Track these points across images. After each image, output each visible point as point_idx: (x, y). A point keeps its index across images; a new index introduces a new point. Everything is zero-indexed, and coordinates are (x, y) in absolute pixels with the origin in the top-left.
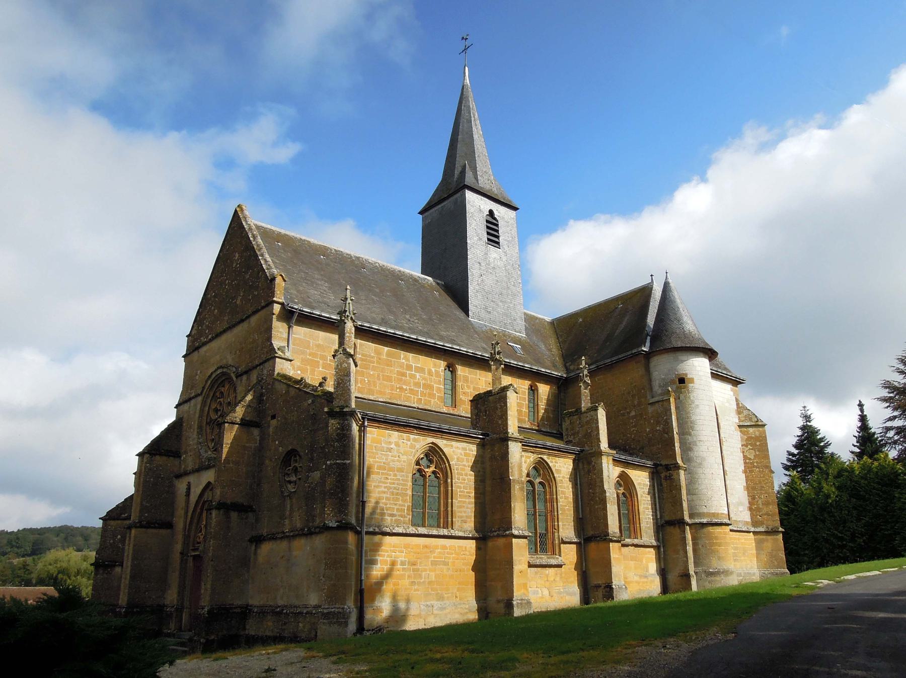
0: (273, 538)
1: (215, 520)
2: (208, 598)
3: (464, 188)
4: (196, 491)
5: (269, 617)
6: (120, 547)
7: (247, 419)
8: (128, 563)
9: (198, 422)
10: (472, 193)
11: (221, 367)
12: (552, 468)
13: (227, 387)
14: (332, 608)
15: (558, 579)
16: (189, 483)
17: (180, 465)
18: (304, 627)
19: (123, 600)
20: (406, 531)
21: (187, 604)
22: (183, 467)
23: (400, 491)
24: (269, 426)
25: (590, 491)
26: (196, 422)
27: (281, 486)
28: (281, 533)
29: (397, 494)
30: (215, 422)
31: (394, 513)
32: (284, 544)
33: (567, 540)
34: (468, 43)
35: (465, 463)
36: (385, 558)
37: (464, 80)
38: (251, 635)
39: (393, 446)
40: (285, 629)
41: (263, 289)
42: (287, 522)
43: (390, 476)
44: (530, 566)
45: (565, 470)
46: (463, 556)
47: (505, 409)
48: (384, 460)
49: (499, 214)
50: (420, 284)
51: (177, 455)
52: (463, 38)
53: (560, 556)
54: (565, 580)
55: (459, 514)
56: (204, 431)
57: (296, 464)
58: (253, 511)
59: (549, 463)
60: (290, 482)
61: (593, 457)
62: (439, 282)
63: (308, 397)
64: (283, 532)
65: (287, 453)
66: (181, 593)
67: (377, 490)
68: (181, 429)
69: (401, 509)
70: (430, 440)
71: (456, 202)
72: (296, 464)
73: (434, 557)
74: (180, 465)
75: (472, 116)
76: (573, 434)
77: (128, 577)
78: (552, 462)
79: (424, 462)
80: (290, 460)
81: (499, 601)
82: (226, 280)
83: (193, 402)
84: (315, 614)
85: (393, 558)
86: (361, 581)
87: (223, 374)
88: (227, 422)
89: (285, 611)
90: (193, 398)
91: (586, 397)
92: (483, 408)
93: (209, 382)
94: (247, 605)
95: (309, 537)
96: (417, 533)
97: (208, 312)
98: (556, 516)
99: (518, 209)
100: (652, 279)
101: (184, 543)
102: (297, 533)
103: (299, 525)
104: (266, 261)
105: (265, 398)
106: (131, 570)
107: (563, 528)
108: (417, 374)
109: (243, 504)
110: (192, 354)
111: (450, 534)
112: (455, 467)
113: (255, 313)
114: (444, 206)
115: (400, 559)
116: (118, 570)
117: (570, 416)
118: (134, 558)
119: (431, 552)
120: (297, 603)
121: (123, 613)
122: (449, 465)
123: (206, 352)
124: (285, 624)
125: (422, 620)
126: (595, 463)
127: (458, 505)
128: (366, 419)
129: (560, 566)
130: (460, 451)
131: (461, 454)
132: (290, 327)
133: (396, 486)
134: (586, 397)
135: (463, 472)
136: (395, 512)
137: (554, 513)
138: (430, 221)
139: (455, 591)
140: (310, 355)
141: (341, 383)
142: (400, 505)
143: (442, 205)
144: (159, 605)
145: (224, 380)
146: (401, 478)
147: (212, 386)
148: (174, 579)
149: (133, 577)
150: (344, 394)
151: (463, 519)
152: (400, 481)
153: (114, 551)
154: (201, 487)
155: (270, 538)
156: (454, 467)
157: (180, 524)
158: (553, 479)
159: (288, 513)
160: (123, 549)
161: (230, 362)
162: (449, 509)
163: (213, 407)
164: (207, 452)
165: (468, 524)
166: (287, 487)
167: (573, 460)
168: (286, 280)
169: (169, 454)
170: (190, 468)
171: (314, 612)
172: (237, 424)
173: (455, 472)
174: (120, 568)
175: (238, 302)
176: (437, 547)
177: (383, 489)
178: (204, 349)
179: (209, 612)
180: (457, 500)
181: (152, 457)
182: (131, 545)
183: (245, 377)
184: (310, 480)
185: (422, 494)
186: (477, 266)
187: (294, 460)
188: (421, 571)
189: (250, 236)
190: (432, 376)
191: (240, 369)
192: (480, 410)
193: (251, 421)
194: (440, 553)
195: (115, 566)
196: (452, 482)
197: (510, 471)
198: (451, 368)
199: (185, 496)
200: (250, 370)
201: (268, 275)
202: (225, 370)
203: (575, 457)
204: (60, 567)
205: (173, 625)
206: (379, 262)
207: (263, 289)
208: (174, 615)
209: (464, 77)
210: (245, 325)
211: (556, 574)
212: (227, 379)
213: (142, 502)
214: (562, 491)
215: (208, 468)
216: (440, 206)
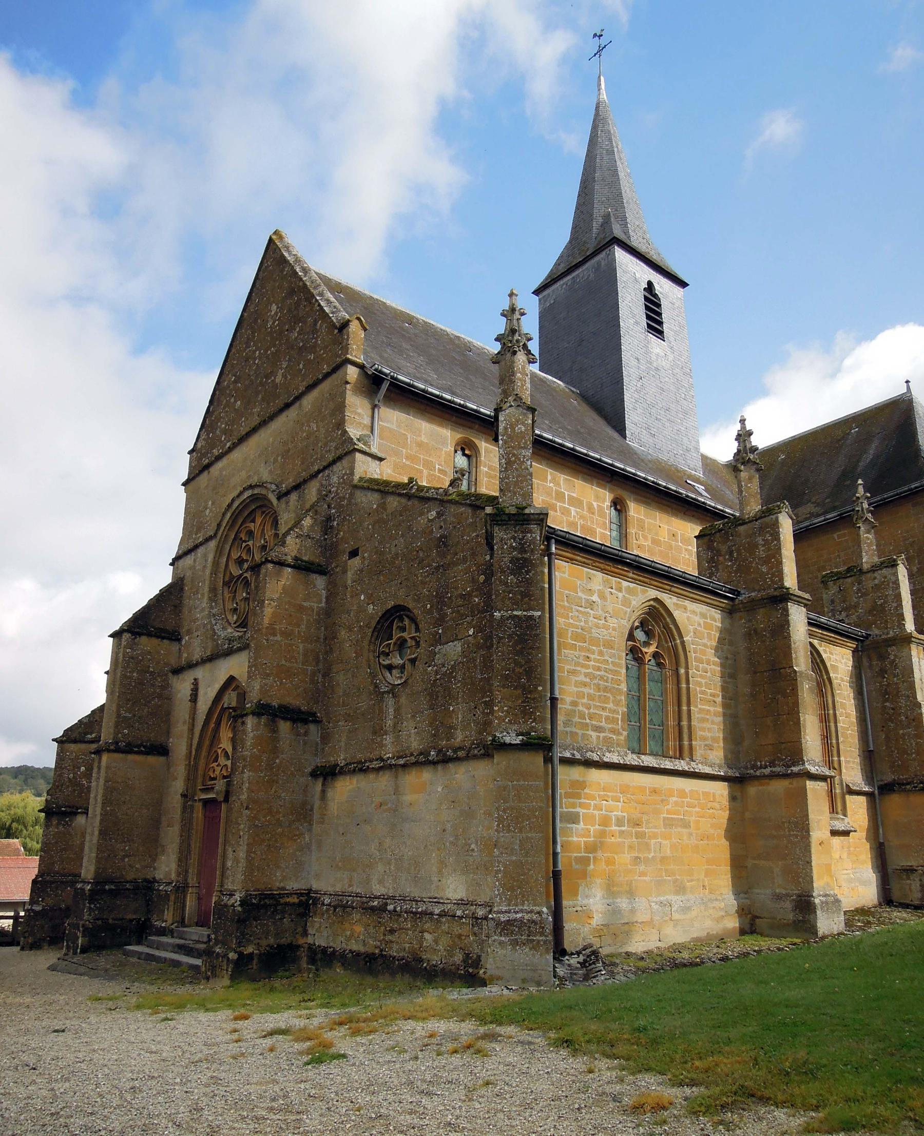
0: (361, 770)
1: (251, 735)
2: (240, 877)
3: (612, 244)
4: (207, 695)
5: (356, 916)
7: (305, 558)
8: (96, 808)
9: (211, 581)
10: (624, 253)
11: (251, 487)
12: (826, 661)
13: (259, 520)
14: (516, 913)
15: (845, 856)
16: (195, 679)
17: (180, 652)
18: (436, 941)
19: (88, 870)
20: (625, 760)
21: (192, 880)
22: (185, 655)
23: (609, 684)
24: (345, 572)
25: (887, 704)
26: (207, 583)
27: (373, 676)
28: (377, 760)
29: (606, 689)
30: (238, 579)
31: (602, 724)
32: (384, 781)
33: (855, 788)
34: (603, 41)
35: (705, 641)
36: (591, 811)
37: (599, 94)
38: (319, 946)
39: (595, 598)
40: (391, 942)
41: (326, 347)
42: (388, 740)
43: (593, 653)
44: (834, 833)
45: (843, 667)
46: (711, 811)
47: (775, 545)
48: (582, 624)
49: (660, 290)
50: (549, 386)
51: (174, 636)
53: (845, 815)
54: (855, 858)
55: (701, 733)
56: (220, 597)
57: (405, 635)
58: (317, 721)
59: (822, 653)
60: (390, 668)
61: (890, 646)
62: (572, 389)
63: (427, 508)
64: (382, 759)
65: (383, 615)
66: (183, 859)
67: (574, 678)
68: (181, 597)
69: (613, 717)
70: (653, 593)
71: (598, 268)
72: (405, 635)
73: (668, 812)
74: (180, 652)
75: (614, 145)
76: (846, 609)
77: (96, 833)
78: (825, 651)
79: (640, 635)
80: (390, 626)
81: (778, 897)
82: (255, 352)
83: (201, 551)
84: (461, 918)
85: (604, 812)
86: (555, 854)
87: (254, 498)
88: (272, 562)
89: (390, 907)
90: (201, 544)
91: (869, 545)
92: (724, 548)
93: (229, 515)
95: (440, 767)
96: (642, 764)
97: (224, 408)
98: (835, 745)
99: (688, 285)
100: (908, 388)
101: (188, 779)
102: (413, 759)
103: (415, 744)
104: (329, 302)
105: (335, 523)
106: (102, 820)
107: (846, 767)
108: (572, 509)
109: (300, 710)
110: (197, 479)
111: (692, 770)
112: (692, 646)
113: (311, 387)
114: (578, 275)
115: (615, 813)
116: (80, 820)
117: (838, 579)
119: (662, 801)
120: (416, 893)
121: (87, 892)
122: (683, 643)
123: (221, 470)
124: (392, 931)
125: (654, 931)
126: (895, 656)
127: (699, 716)
128: (553, 541)
129: (846, 833)
130: (697, 618)
131: (699, 625)
132: (374, 407)
133: (602, 673)
134: (869, 545)
135: (704, 657)
136: (603, 724)
137: (831, 739)
138: (552, 302)
139: (702, 876)
140: (407, 458)
141: (515, 462)
142: (611, 711)
143: (574, 274)
144: (146, 880)
145: (254, 510)
146: (610, 660)
148: (171, 836)
149: (103, 833)
150: (522, 482)
151: (707, 743)
152: (608, 665)
153: (74, 790)
154: (217, 686)
155: (354, 770)
156: (691, 647)
157: (180, 746)
158: (826, 681)
159: (389, 723)
160: (89, 788)
161: (266, 476)
162: (684, 723)
163: (235, 555)
164: (226, 630)
165: (714, 753)
166: (384, 678)
167: (853, 652)
168: (367, 327)
169: (163, 635)
170: (196, 657)
171: (459, 913)
172: (289, 566)
173: (692, 656)
174: (85, 816)
175: (279, 379)
176: (670, 793)
177: (582, 678)
178: (219, 465)
179: (243, 903)
180: (696, 707)
181: (136, 638)
182: (102, 781)
183: (294, 497)
184: (438, 659)
185: (638, 694)
186: (635, 363)
187: (398, 627)
188: (650, 838)
189: (298, 270)
190: (593, 513)
191: (284, 486)
192: (719, 551)
193: (311, 563)
194: (676, 803)
195: (76, 814)
196: (687, 674)
197: (794, 656)
198: (618, 505)
199: (190, 701)
200: (305, 481)
201: (335, 321)
202: (256, 491)
203: (857, 645)
204: (15, 814)
206: (487, 348)
207: (326, 347)
208: (172, 898)
209: (599, 90)
210: (292, 412)
211: (843, 847)
212: (260, 507)
213: (118, 711)
214: (841, 702)
215: (229, 653)
216: (569, 277)
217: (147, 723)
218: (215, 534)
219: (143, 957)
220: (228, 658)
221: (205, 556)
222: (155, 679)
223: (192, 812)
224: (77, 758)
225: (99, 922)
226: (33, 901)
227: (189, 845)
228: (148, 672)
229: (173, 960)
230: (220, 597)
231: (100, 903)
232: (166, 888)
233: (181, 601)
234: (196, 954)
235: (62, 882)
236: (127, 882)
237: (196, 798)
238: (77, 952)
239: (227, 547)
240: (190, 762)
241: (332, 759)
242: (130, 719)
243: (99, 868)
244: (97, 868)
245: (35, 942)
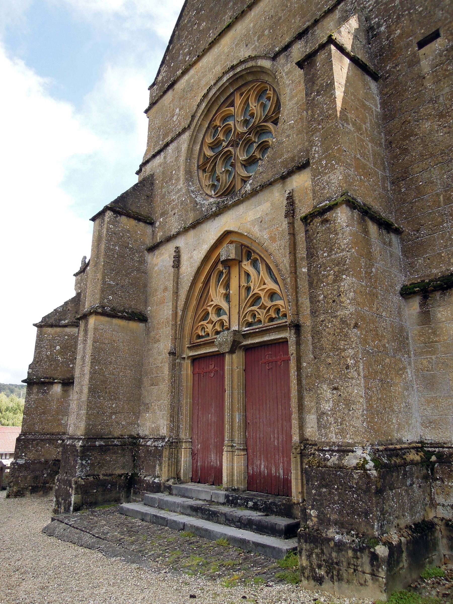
6: (59, 360)
16: (177, 248)
21: (184, 435)
56: (196, 178)
68: (152, 190)
77: (86, 390)
83: (170, 149)
93: (204, 105)
94: (421, 442)
106: (91, 379)
118: (94, 361)
121: (78, 449)
145: (232, 94)
147: (208, 110)
153: (51, 365)
181: (117, 217)
182: (90, 342)
195: (52, 383)
205: (165, 469)
213: (104, 278)
217: (128, 292)
218: (189, 126)
219: (148, 518)
220: (217, 219)
221: (178, 150)
222: (134, 254)
223: (180, 369)
224: (54, 339)
225: (91, 479)
226: (16, 455)
227: (179, 400)
228: (127, 247)
229: (198, 529)
230: (196, 178)
231: (91, 460)
232: (156, 444)
233: (152, 193)
234: (222, 519)
235: (42, 440)
236: (115, 438)
237: (184, 356)
238: (69, 509)
239: (201, 136)
240: (176, 322)
241: (434, 271)
242: (113, 287)
243: (89, 425)
244: (88, 425)
245: (19, 491)
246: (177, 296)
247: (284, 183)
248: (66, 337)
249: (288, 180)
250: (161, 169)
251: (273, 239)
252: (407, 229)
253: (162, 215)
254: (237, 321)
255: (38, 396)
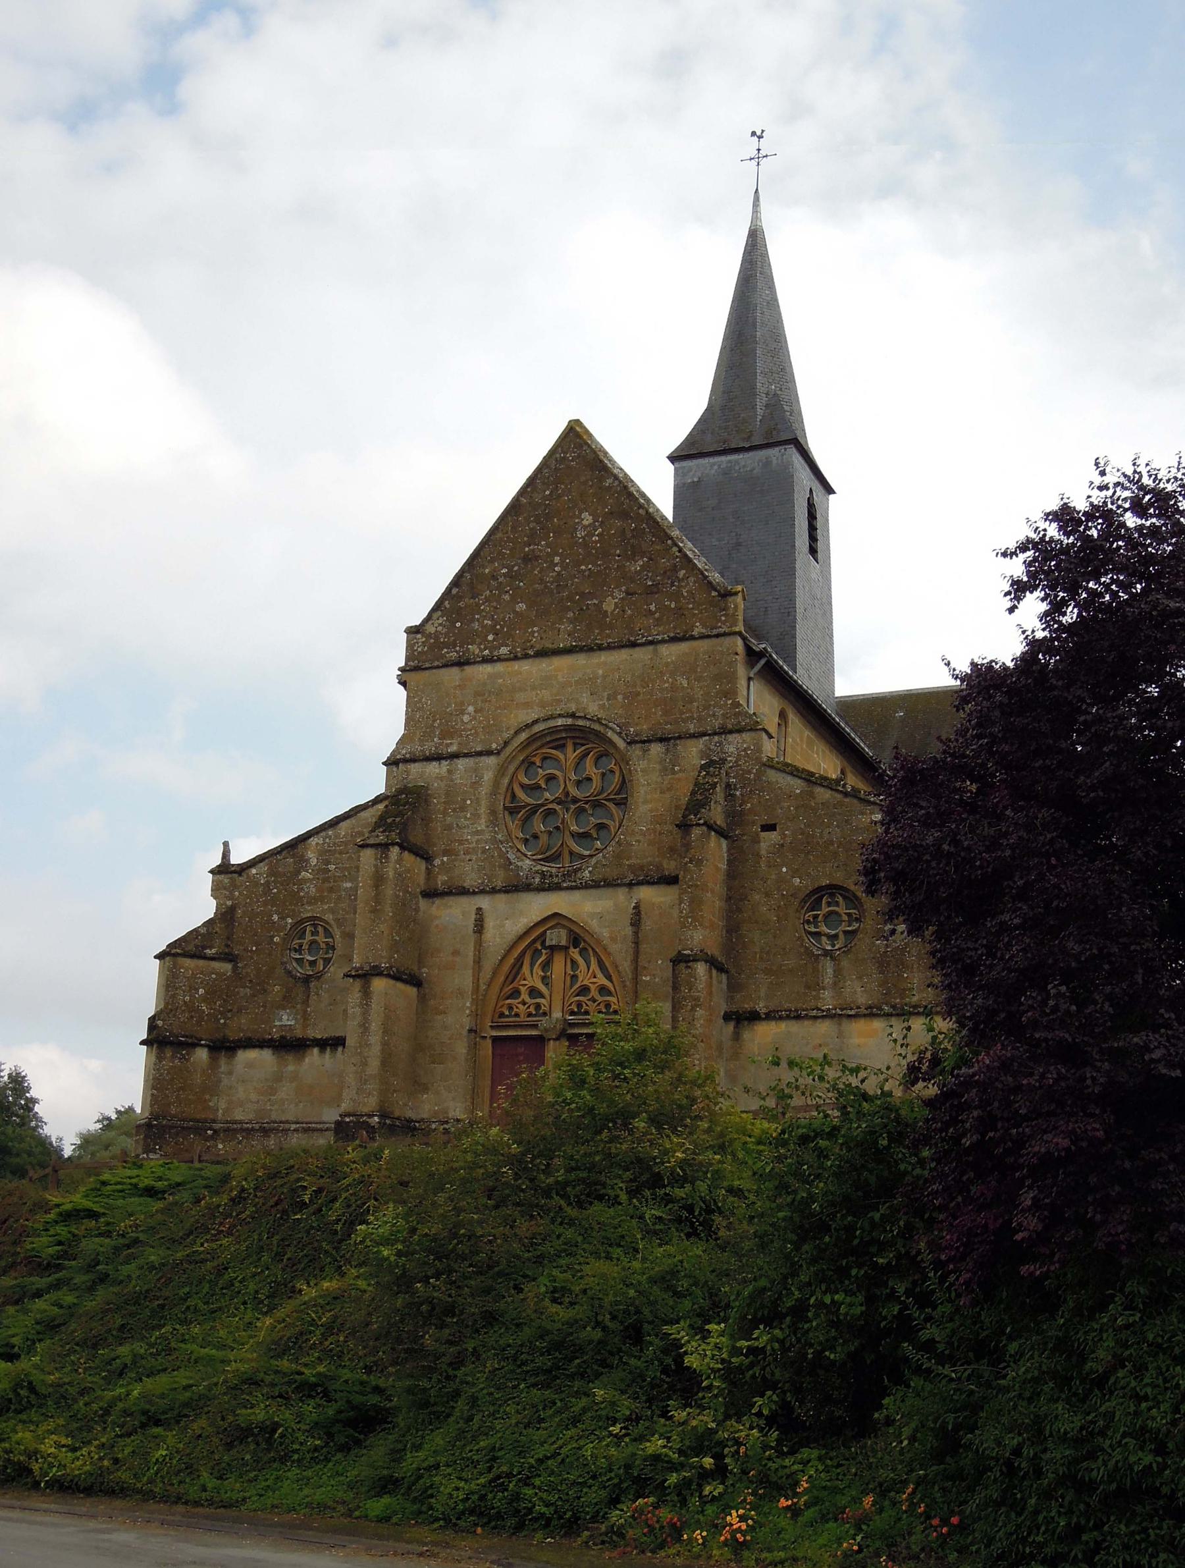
3: (790, 444)
52: (754, 134)
71: (767, 463)
103: (862, 999)
138: (696, 480)
153: (192, 1017)
195: (195, 1046)
235: (183, 1128)
239: (512, 769)
241: (746, 1006)
246: (480, 967)
247: (630, 889)
248: (214, 976)
249: (635, 889)
250: (443, 784)
251: (613, 939)
252: (733, 971)
253: (446, 852)
254: (560, 1007)
255: (173, 1062)
